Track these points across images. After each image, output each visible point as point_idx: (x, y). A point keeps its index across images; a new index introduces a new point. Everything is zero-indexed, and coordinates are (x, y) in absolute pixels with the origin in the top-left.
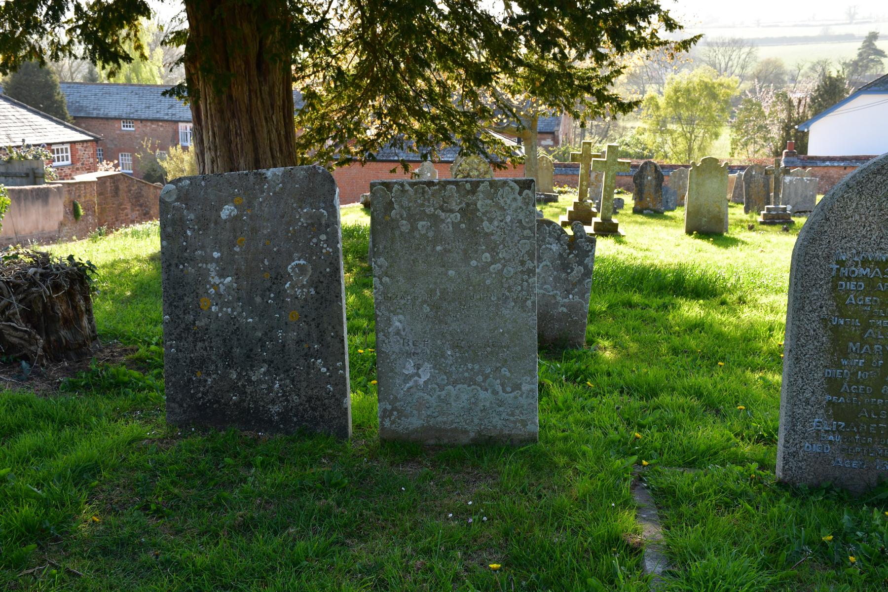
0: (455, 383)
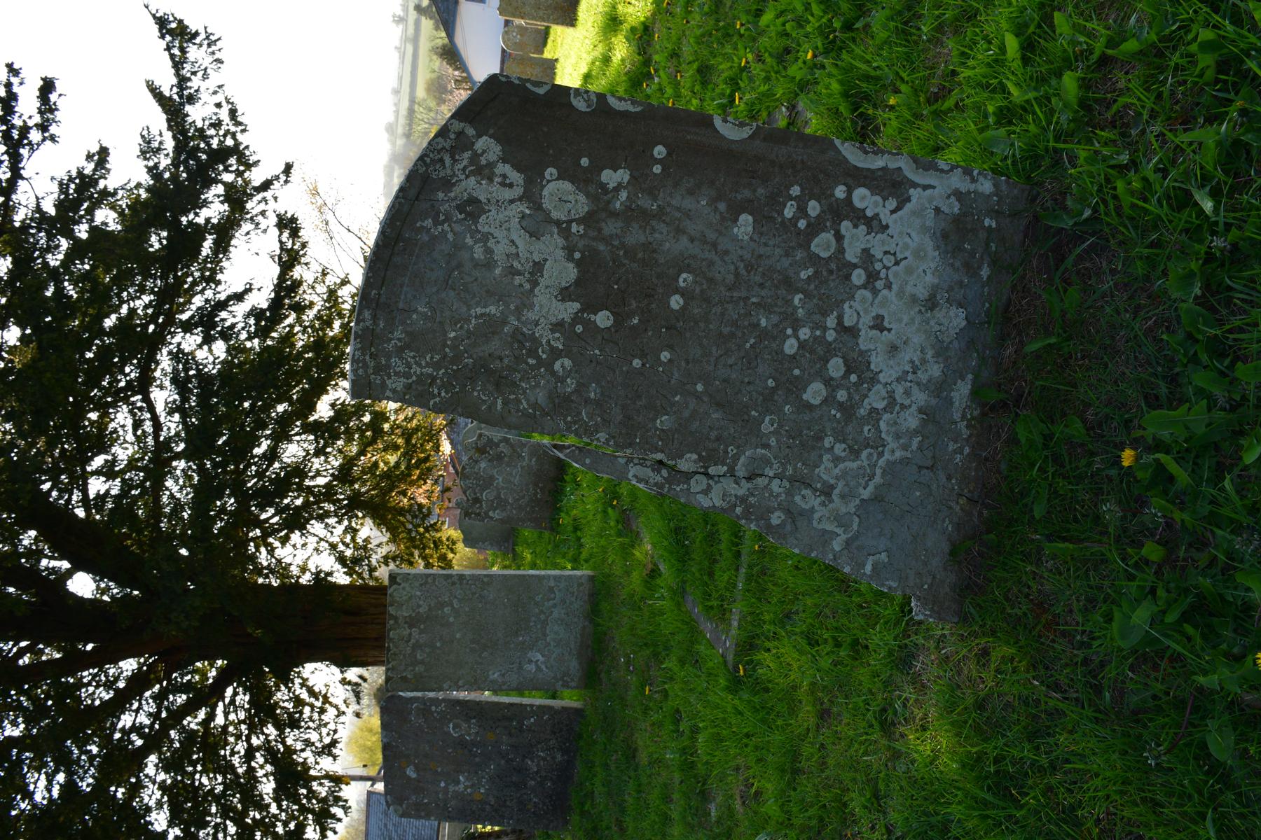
0: (545, 635)
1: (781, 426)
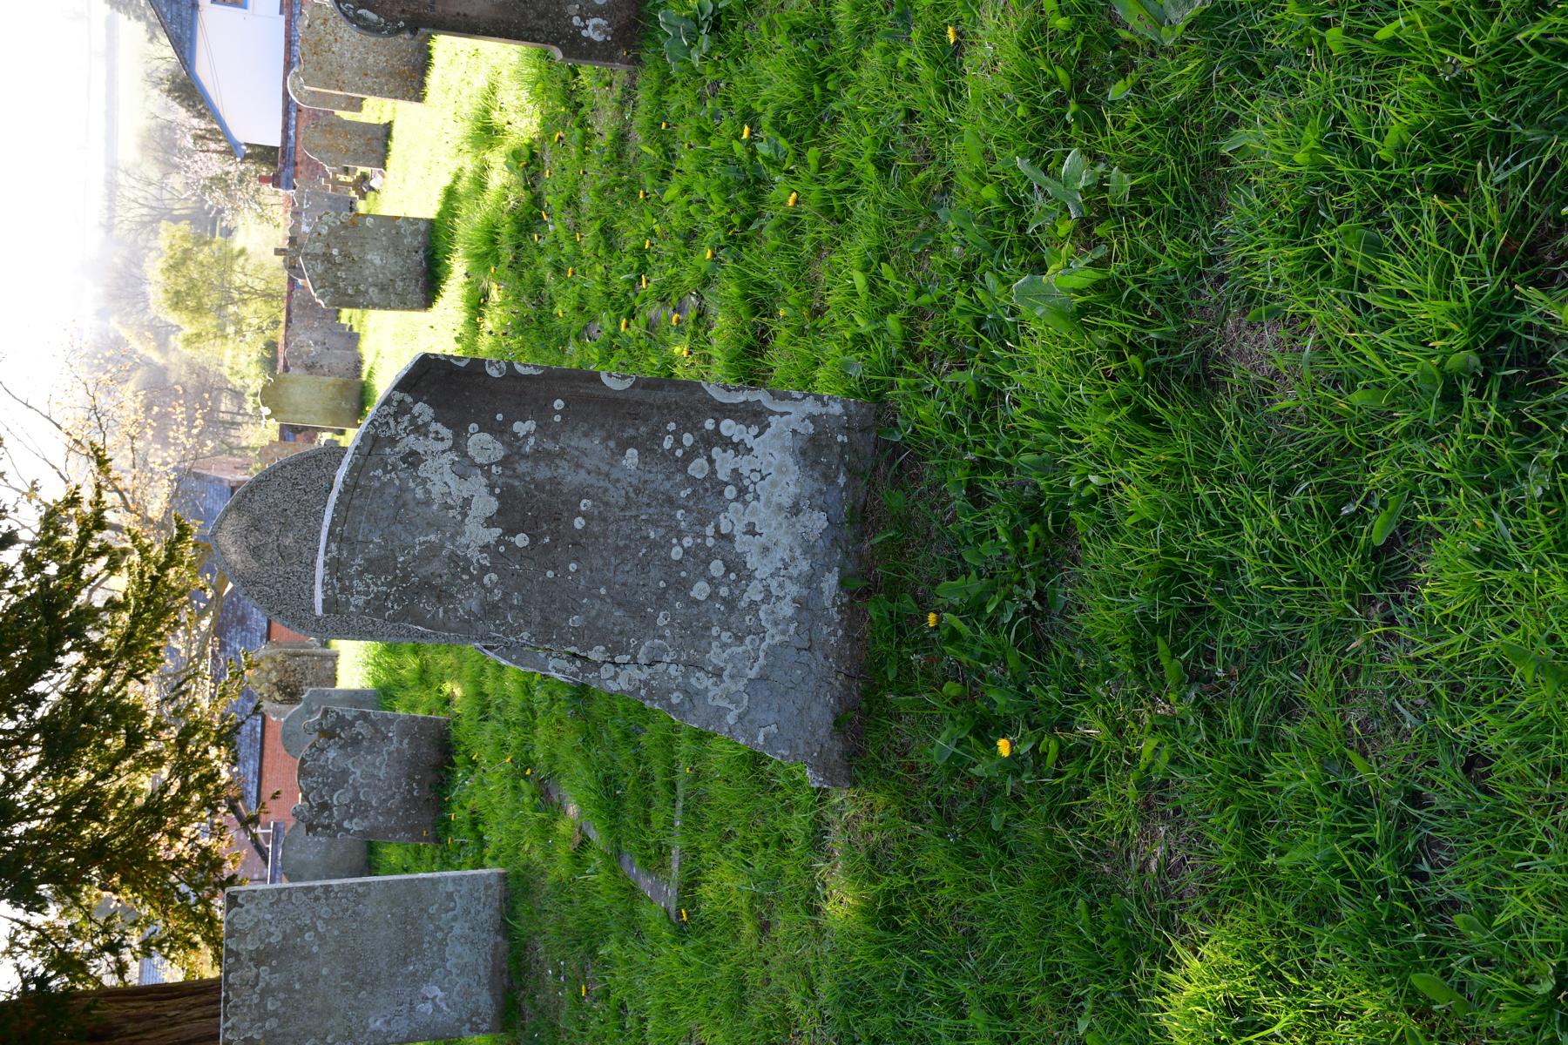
0: (443, 960)
1: (673, 619)
